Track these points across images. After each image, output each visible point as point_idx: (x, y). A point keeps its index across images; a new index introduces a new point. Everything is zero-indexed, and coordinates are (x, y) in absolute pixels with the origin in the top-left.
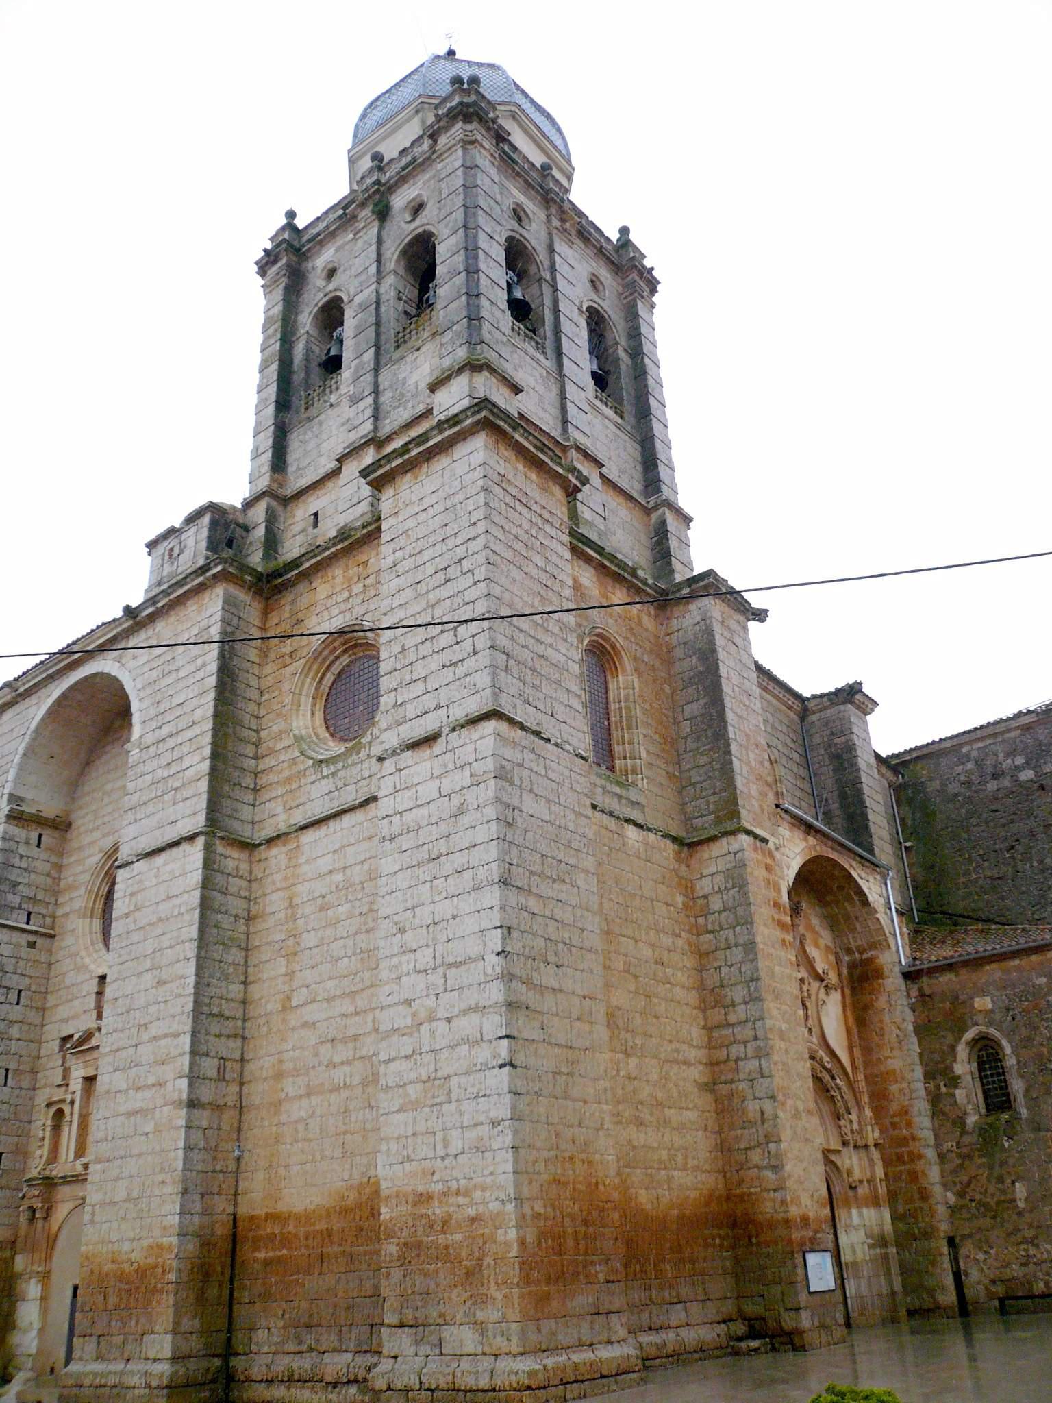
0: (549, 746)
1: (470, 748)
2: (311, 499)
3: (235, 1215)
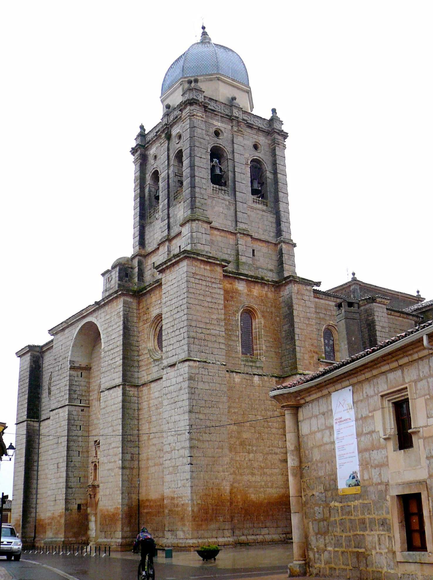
0: (210, 365)
1: (183, 369)
2: (152, 257)
3: (139, 499)
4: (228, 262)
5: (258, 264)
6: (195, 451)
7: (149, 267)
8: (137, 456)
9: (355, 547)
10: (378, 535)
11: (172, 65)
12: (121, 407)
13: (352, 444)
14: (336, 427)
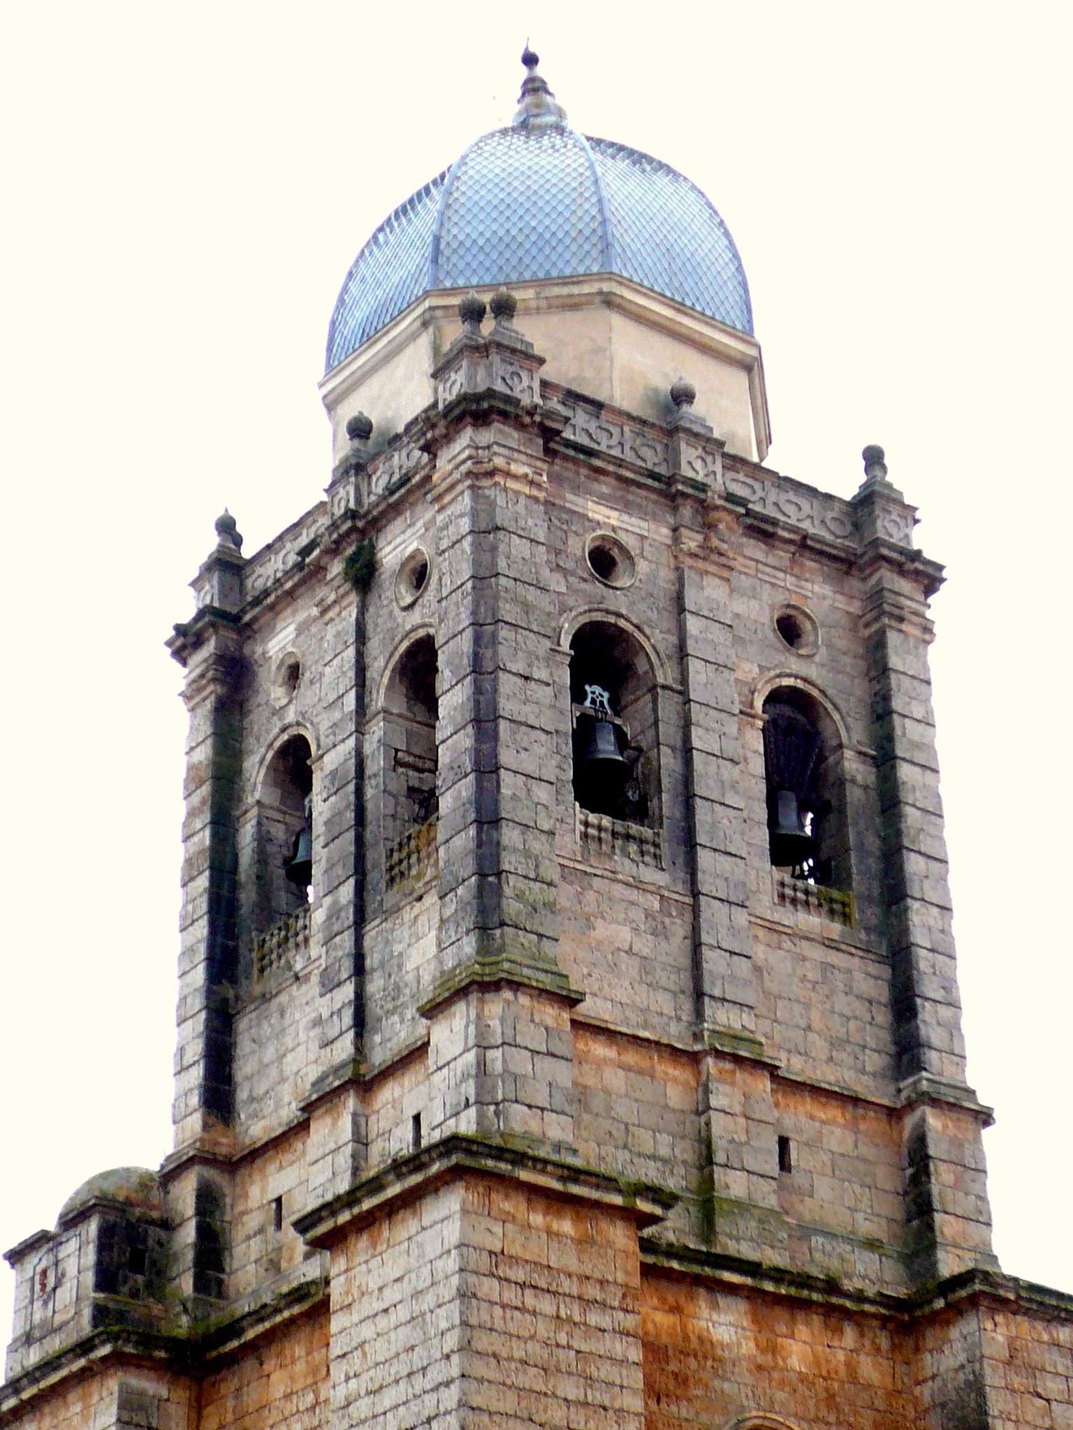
2: (272, 1168)
4: (666, 1199)
5: (808, 1210)
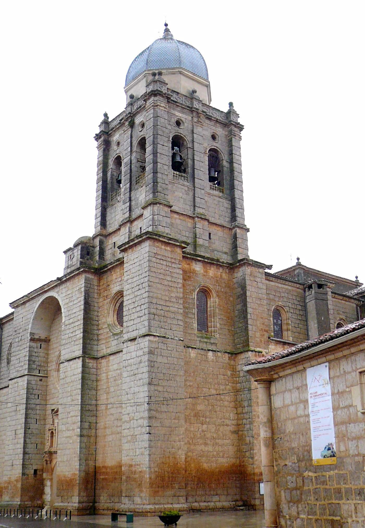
0: (168, 340)
1: (143, 344)
2: (113, 237)
3: (95, 466)
4: (188, 244)
5: (214, 246)
6: (153, 421)
7: (110, 247)
8: (95, 425)
9: (330, 515)
10: (354, 504)
11: (136, 58)
12: (80, 377)
13: (328, 417)
14: (311, 401)
